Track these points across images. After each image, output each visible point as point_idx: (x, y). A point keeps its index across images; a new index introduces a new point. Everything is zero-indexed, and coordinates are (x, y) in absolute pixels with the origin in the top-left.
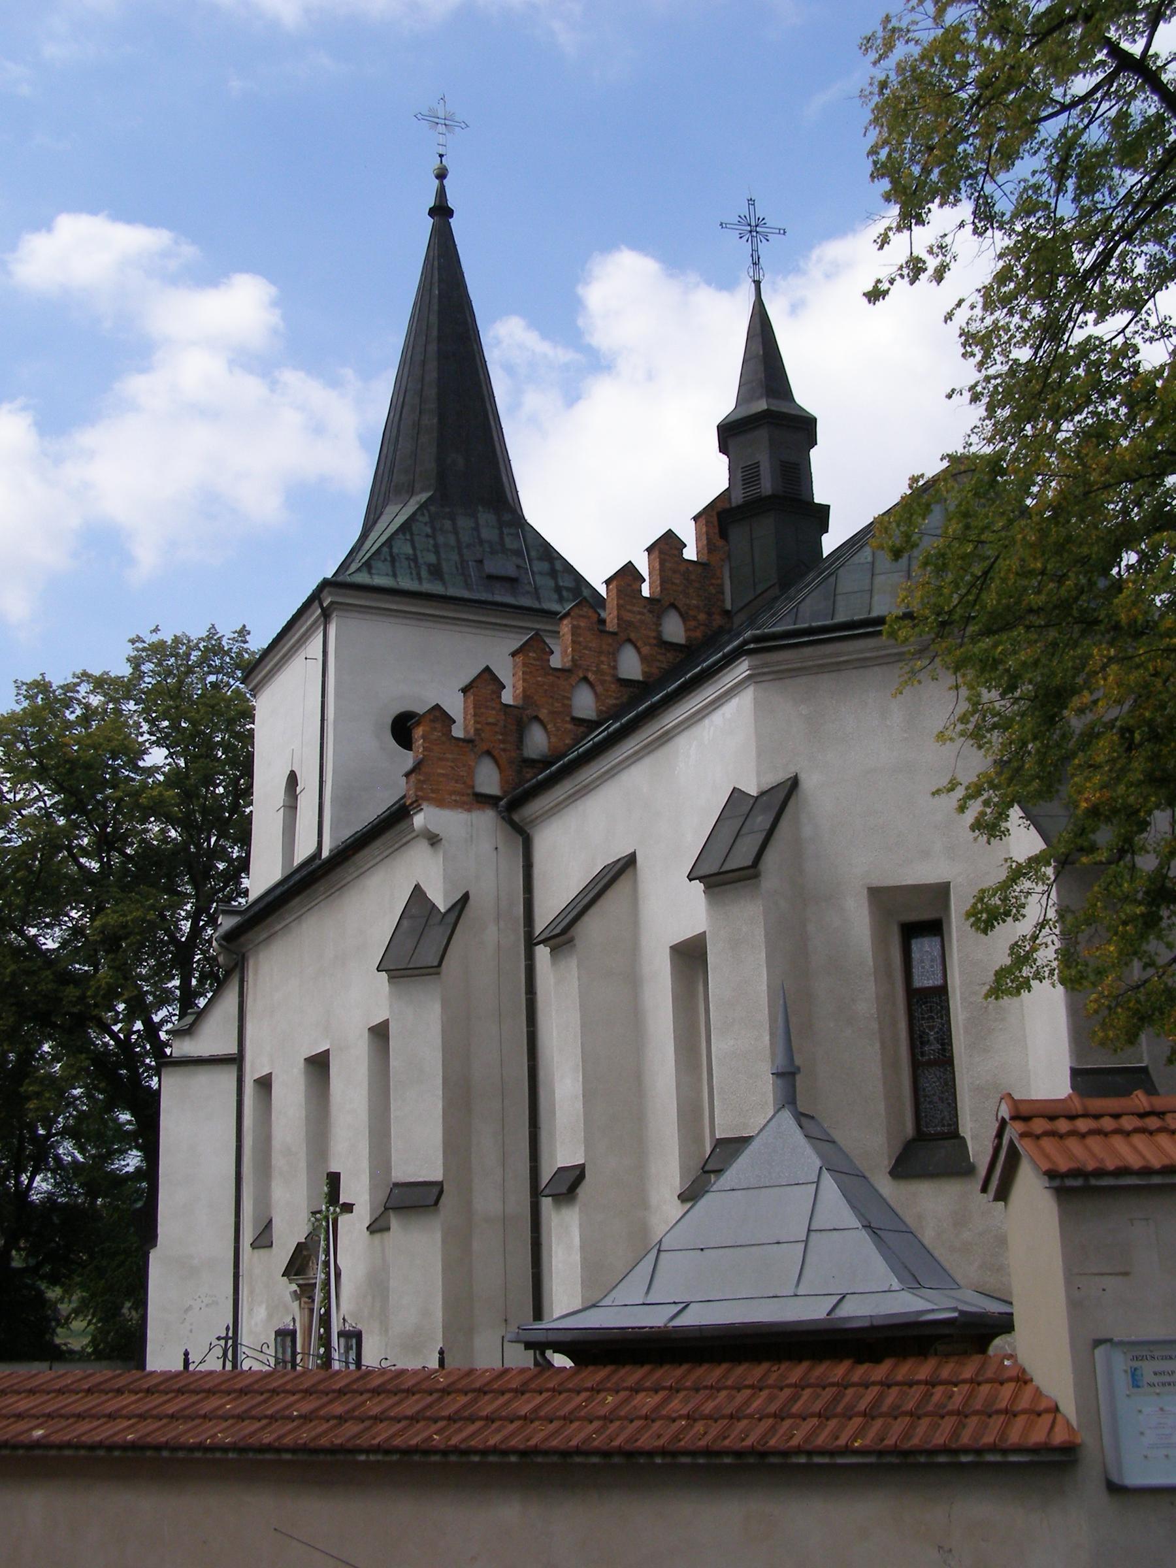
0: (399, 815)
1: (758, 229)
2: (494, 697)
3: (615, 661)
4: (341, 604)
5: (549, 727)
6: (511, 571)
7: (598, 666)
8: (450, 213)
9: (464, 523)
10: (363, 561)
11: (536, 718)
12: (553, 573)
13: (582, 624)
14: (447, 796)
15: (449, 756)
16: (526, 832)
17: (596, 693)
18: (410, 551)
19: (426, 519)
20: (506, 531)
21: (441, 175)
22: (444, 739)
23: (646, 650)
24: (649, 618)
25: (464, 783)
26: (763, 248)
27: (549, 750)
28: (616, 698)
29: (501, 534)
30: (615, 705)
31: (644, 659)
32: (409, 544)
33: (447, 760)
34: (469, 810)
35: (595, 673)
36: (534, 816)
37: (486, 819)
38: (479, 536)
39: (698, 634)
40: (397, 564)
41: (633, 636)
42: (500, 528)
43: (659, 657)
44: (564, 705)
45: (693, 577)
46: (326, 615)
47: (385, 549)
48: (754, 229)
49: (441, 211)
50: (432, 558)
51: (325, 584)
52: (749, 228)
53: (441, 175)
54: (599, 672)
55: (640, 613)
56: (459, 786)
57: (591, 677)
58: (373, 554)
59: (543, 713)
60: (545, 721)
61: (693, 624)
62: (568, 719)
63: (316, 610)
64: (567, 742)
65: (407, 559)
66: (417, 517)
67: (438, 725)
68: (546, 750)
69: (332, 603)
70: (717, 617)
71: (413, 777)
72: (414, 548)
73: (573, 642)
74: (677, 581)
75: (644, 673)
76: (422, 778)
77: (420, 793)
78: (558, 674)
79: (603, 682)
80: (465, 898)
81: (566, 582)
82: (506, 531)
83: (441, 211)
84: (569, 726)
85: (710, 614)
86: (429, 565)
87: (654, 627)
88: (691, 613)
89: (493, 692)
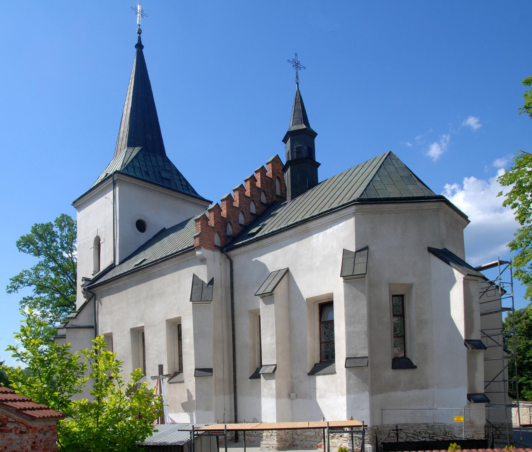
0: (191, 249)
1: (298, 65)
2: (219, 213)
3: (250, 206)
4: (122, 180)
5: (233, 226)
6: (169, 177)
7: (245, 208)
8: (142, 47)
9: (153, 158)
10: (125, 166)
11: (230, 222)
12: (180, 180)
13: (241, 193)
14: (207, 245)
15: (208, 232)
16: (231, 260)
17: (245, 217)
18: (139, 166)
19: (142, 155)
20: (165, 163)
21: (140, 33)
22: (206, 226)
23: (257, 204)
24: (258, 194)
25: (212, 241)
26: (299, 71)
27: (233, 234)
28: (250, 219)
29: (164, 164)
30: (250, 221)
31: (256, 208)
32: (138, 162)
33: (207, 233)
34: (213, 251)
35: (245, 210)
36: (235, 255)
37: (218, 254)
38: (158, 164)
39: (270, 202)
40: (135, 169)
41: (254, 199)
42: (164, 162)
43: (261, 207)
44: (237, 219)
45: (269, 182)
46: (114, 184)
47: (131, 163)
48: (297, 65)
49: (139, 46)
50: (146, 169)
51: (117, 172)
52: (295, 64)
53: (140, 33)
54: (246, 210)
55: (256, 192)
56: (211, 243)
57: (244, 211)
58: (128, 164)
59: (232, 221)
60: (232, 223)
61: (268, 198)
62: (238, 224)
63: (111, 180)
64: (238, 231)
65: (138, 168)
66: (139, 154)
67: (205, 221)
68: (232, 233)
69: (117, 179)
70: (274, 197)
71: (198, 239)
72: (140, 164)
73: (239, 199)
74: (265, 183)
75: (256, 212)
76: (201, 238)
77: (201, 243)
78: (235, 209)
79: (247, 213)
80: (213, 279)
81: (184, 183)
82: (165, 163)
83: (139, 46)
84: (239, 227)
85: (273, 196)
86: (145, 171)
87: (259, 197)
88: (268, 194)
89: (219, 212)
